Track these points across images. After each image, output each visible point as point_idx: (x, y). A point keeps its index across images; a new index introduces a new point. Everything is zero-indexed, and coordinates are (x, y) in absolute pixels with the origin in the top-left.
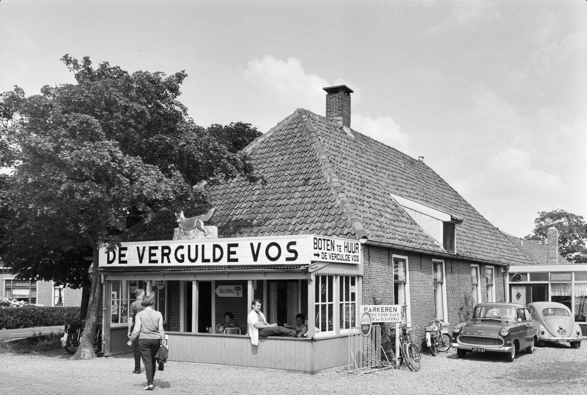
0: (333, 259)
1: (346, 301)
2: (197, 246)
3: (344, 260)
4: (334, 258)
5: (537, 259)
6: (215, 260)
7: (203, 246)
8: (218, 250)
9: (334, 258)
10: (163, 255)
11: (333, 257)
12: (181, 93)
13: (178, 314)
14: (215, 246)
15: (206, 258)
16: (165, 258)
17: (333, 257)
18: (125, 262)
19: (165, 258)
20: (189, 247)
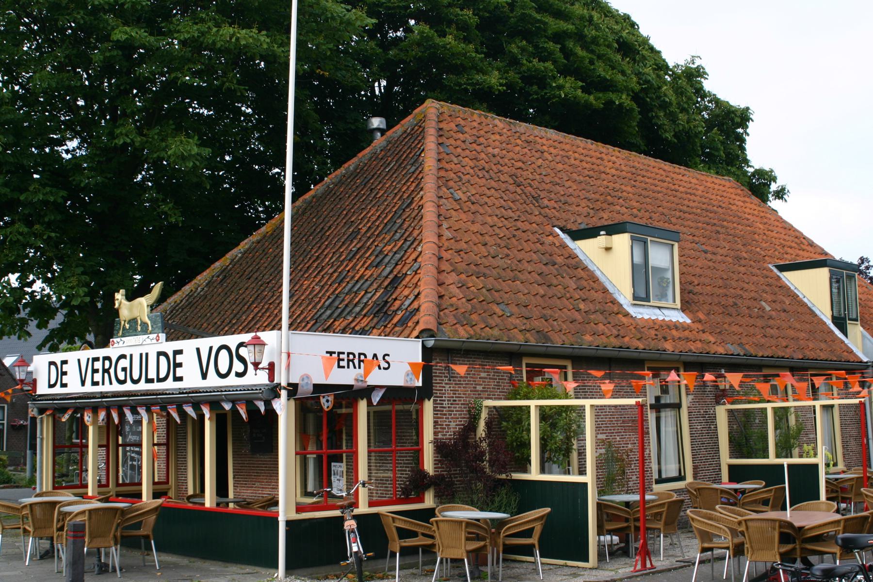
0: (95, 383)
1: (328, 448)
2: (141, 355)
3: (149, 381)
4: (98, 377)
5: (738, 198)
6: (160, 380)
7: (147, 354)
8: (107, 363)
9: (98, 377)
10: (349, 361)
11: (95, 371)
12: (863, 260)
13: (185, 449)
14: (160, 354)
15: (149, 377)
16: (351, 363)
17: (95, 371)
18: (180, 379)
19: (351, 363)
20: (131, 356)
